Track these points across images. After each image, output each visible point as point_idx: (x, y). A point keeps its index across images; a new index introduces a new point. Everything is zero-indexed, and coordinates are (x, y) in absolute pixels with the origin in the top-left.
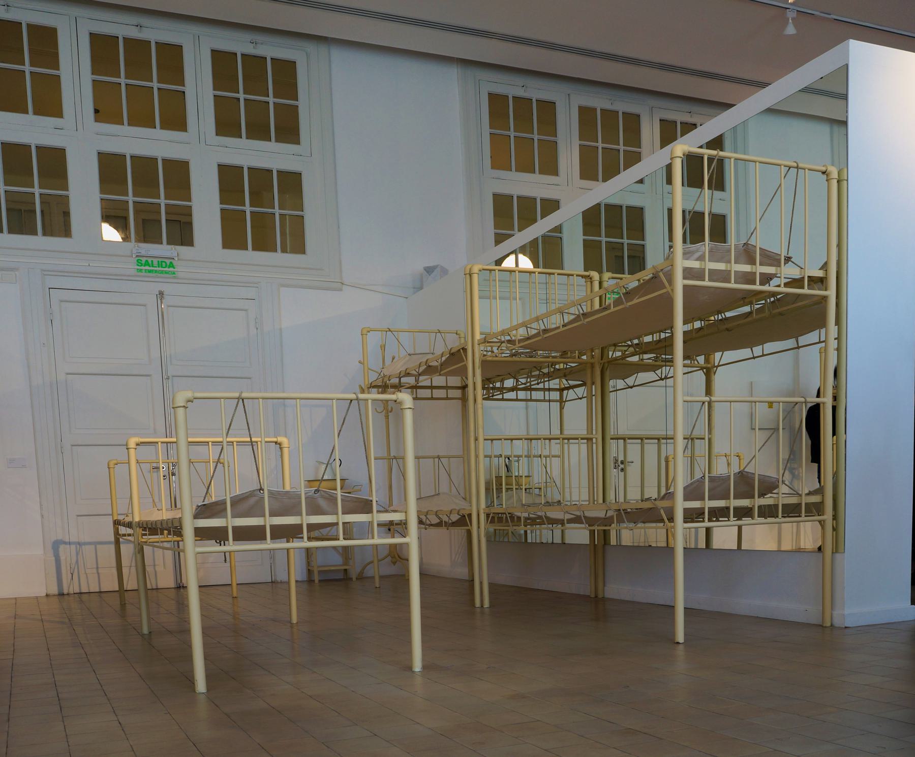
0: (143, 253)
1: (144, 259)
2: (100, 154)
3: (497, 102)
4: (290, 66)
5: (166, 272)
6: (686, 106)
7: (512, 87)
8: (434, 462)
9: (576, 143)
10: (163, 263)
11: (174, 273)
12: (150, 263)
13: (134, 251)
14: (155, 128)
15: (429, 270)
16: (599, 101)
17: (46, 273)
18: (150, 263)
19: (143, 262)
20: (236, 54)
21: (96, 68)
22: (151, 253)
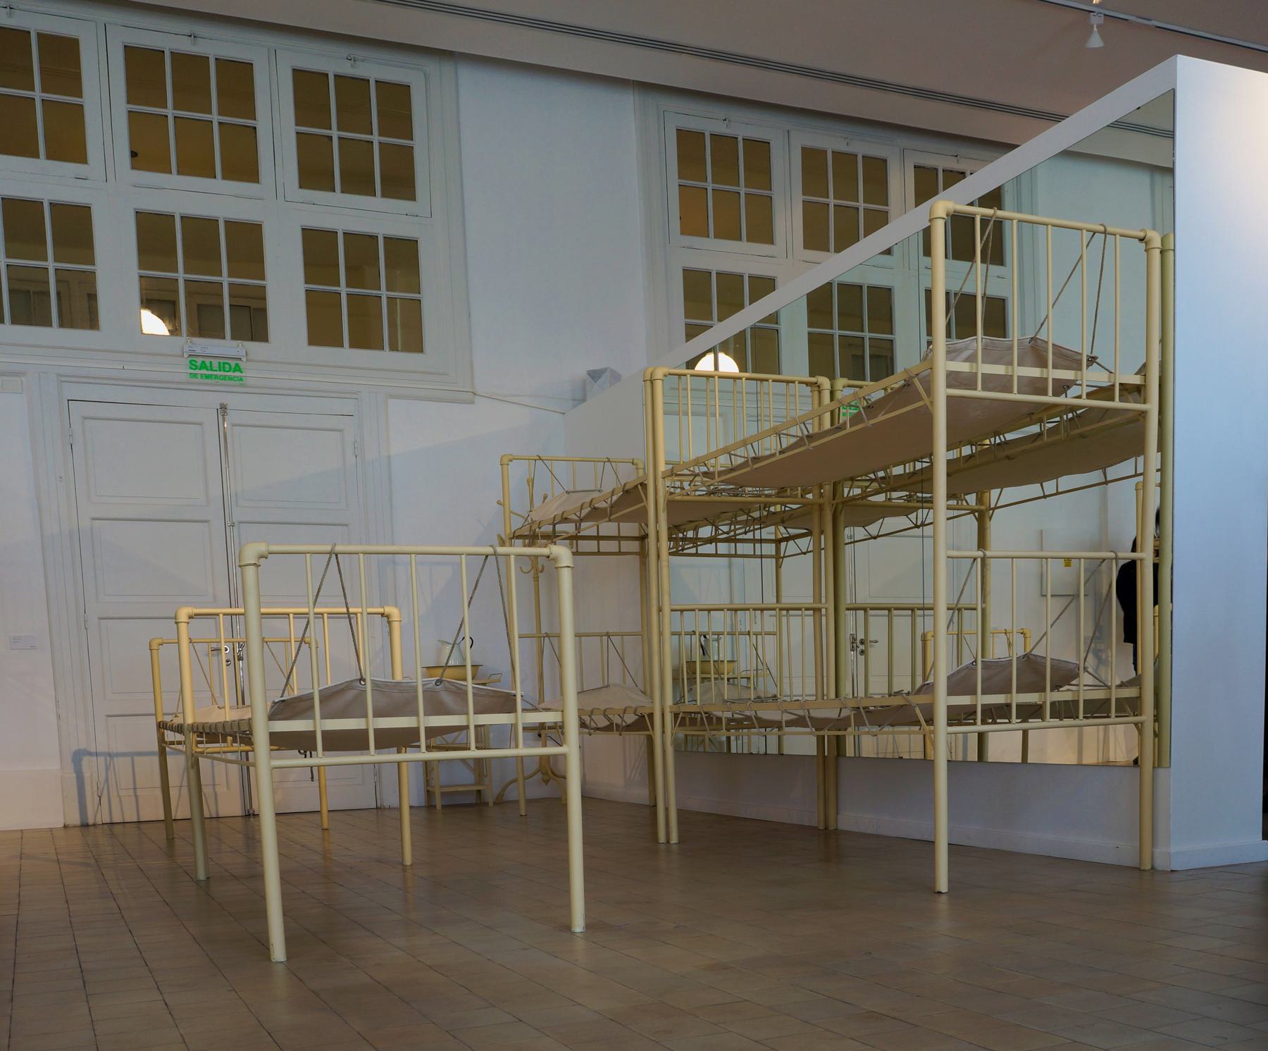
0: (199, 351)
1: (199, 360)
2: (138, 213)
3: (689, 142)
4: (402, 92)
5: (230, 378)
6: (951, 148)
7: (710, 121)
8: (602, 641)
9: (799, 198)
10: (227, 366)
11: (241, 380)
12: (208, 364)
13: (186, 349)
14: (215, 177)
15: (595, 375)
16: (830, 141)
17: (63, 379)
18: (208, 364)
19: (199, 364)
20: (327, 75)
21: (133, 95)
22: (210, 351)
